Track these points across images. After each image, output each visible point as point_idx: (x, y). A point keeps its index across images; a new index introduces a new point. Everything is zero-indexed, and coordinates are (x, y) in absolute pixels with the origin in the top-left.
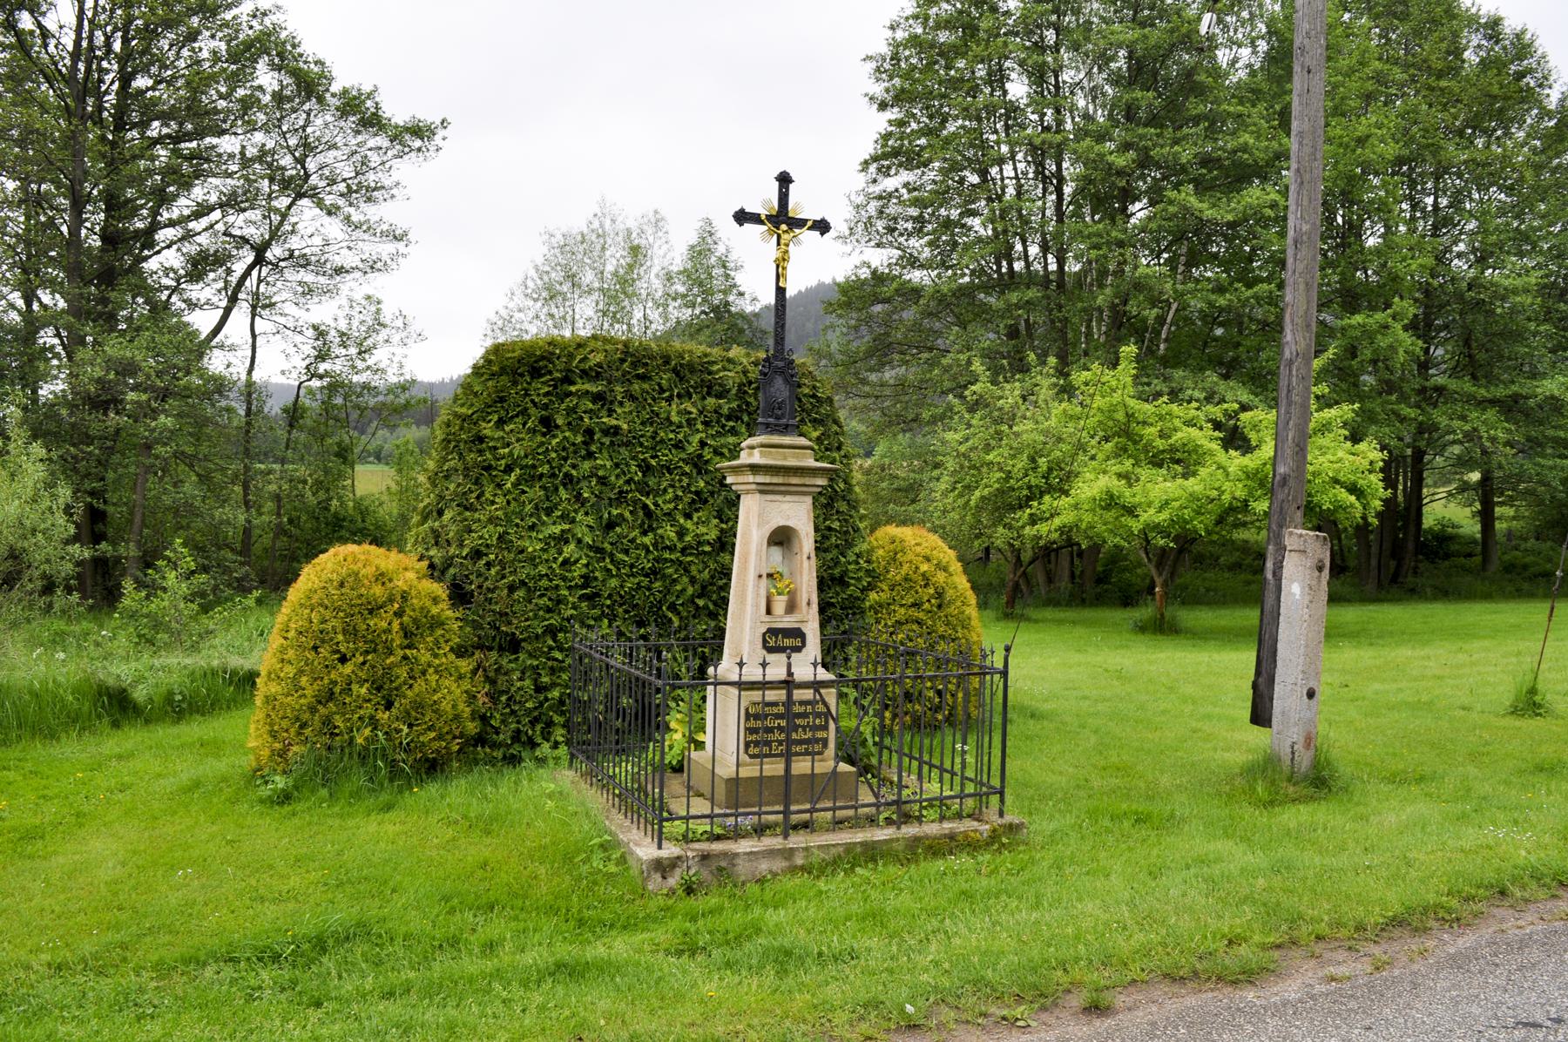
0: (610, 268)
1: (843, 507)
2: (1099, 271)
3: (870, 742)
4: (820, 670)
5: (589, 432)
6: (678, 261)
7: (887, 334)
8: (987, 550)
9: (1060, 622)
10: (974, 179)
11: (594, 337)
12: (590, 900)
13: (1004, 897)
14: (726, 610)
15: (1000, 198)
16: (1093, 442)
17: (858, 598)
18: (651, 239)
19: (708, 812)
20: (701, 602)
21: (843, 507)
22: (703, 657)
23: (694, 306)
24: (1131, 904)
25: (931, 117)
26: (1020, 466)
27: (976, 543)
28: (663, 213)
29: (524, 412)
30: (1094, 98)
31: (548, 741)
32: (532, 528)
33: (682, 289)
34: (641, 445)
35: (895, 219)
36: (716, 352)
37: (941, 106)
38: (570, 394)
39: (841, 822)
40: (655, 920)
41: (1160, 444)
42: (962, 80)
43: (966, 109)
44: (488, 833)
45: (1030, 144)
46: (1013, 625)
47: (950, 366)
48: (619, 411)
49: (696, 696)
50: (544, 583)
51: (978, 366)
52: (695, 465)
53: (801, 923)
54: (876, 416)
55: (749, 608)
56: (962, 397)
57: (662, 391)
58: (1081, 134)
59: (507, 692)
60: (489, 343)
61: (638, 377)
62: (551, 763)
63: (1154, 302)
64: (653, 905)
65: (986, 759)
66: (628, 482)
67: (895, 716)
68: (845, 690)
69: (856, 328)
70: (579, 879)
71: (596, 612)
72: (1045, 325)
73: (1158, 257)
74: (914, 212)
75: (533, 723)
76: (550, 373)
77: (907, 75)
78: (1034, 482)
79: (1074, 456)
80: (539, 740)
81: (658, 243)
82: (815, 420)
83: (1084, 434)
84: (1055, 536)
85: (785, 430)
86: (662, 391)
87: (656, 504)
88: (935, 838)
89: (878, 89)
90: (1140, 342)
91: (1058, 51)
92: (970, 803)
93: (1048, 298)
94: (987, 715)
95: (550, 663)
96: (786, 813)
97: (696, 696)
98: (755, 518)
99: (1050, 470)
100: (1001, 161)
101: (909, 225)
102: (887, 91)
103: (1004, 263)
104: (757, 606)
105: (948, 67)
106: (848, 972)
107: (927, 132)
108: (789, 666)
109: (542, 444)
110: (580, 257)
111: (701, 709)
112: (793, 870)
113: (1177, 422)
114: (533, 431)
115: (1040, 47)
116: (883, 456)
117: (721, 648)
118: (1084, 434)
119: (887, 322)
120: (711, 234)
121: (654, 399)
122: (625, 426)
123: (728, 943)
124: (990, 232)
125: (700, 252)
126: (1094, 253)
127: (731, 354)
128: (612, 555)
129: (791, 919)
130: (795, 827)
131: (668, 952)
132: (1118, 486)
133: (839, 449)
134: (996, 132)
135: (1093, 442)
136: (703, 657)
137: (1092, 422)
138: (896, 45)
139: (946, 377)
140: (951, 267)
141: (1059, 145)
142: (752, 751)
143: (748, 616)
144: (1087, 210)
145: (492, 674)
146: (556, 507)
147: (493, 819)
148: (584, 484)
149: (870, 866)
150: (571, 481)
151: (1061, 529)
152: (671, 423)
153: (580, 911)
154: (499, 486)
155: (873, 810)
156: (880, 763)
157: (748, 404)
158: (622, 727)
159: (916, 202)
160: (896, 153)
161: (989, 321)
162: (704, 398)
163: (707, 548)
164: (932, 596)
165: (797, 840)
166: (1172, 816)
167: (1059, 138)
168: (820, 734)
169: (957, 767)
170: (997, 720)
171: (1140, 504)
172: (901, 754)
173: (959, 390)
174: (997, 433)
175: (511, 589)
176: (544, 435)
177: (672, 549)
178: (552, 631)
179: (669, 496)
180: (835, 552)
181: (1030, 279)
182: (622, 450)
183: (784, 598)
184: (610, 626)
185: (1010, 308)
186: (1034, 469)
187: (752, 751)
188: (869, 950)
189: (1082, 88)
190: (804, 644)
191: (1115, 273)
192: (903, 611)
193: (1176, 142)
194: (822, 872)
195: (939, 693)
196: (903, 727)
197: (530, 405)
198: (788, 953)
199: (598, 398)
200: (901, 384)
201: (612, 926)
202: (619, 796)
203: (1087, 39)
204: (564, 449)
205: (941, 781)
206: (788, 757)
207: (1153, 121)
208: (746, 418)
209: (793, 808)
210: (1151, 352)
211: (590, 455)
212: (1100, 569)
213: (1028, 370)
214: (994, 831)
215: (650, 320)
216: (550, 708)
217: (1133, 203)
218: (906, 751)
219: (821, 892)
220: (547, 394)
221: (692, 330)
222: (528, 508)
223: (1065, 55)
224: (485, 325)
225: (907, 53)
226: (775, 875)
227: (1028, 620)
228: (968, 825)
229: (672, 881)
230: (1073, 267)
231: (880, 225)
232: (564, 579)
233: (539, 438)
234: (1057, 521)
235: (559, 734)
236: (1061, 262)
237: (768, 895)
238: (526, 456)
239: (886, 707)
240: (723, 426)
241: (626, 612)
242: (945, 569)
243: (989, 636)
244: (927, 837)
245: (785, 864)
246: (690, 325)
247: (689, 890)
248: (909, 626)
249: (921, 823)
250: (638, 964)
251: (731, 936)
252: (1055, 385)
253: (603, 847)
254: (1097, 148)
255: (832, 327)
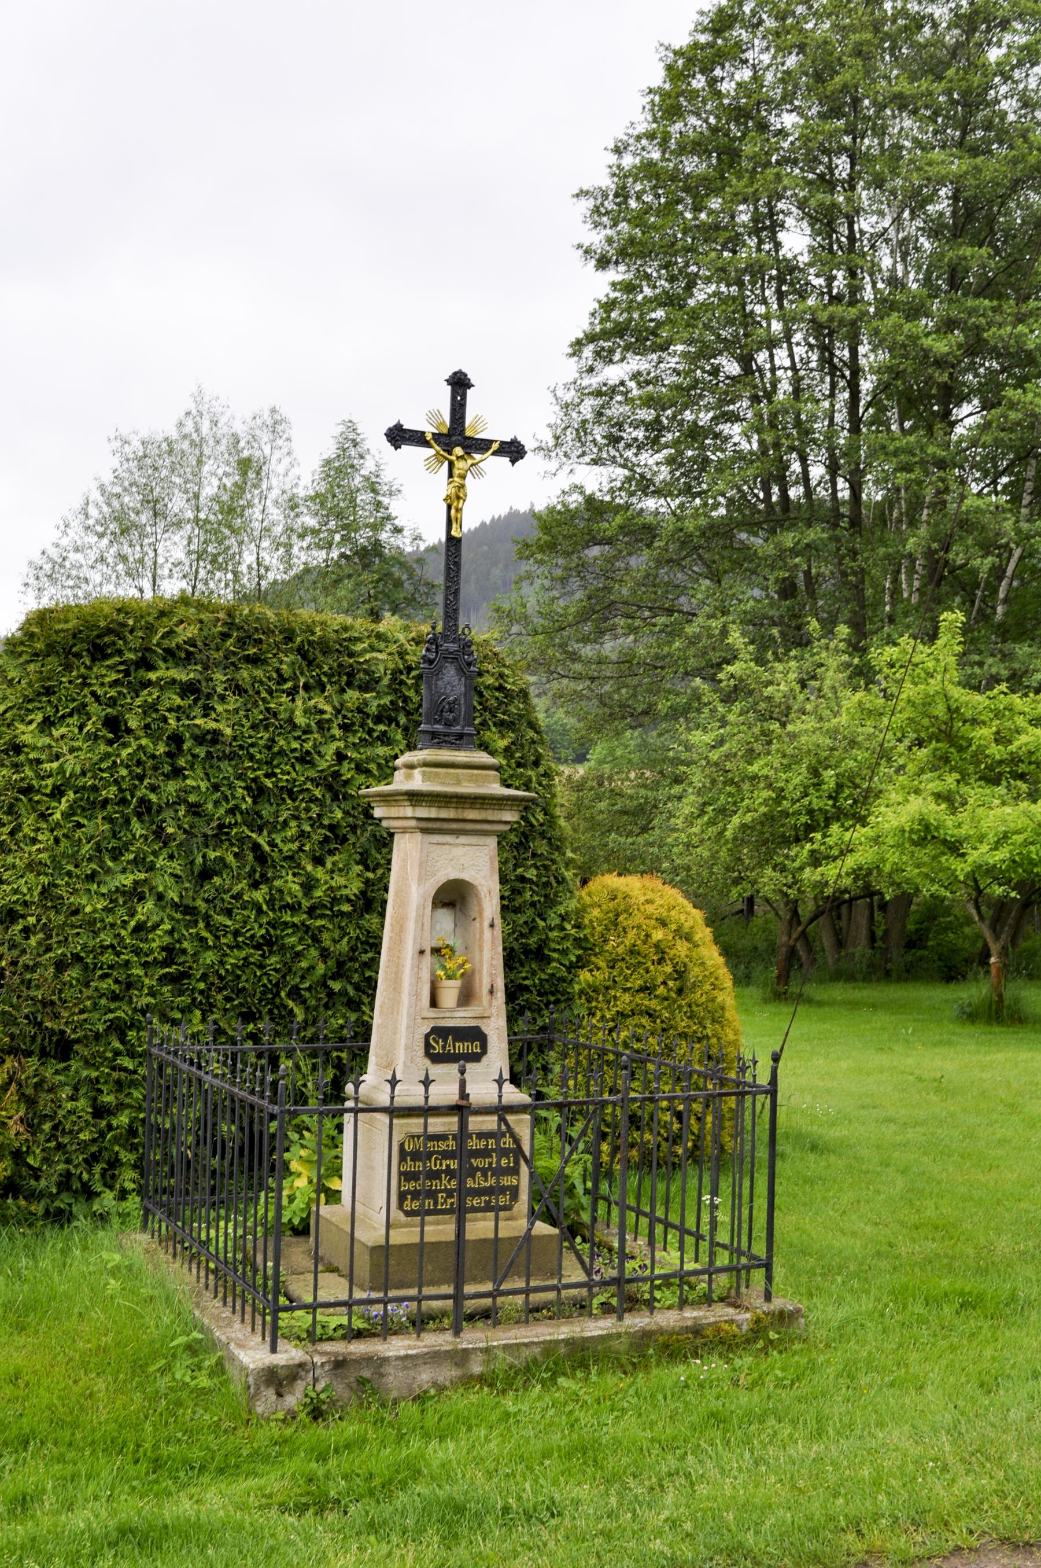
0: (209, 490)
1: (541, 847)
2: (909, 502)
3: (580, 1189)
4: (508, 1088)
5: (176, 739)
6: (306, 480)
7: (608, 589)
8: (751, 901)
9: (854, 1005)
10: (733, 368)
11: (184, 600)
12: (173, 1429)
13: (771, 1422)
14: (373, 997)
15: (769, 395)
16: (901, 748)
17: (563, 980)
18: (267, 450)
19: (344, 1296)
20: (336, 986)
21: (541, 847)
22: (339, 1065)
23: (329, 546)
24: (954, 1431)
25: (672, 279)
26: (796, 781)
27: (735, 892)
28: (284, 412)
29: (81, 709)
30: (905, 255)
31: (111, 1188)
32: (91, 877)
33: (311, 522)
34: (251, 758)
35: (620, 425)
36: (360, 624)
37: (687, 265)
38: (149, 683)
39: (537, 1310)
40: (266, 1459)
41: (996, 751)
42: (717, 227)
43: (723, 270)
44: (21, 1328)
45: (813, 321)
46: (787, 1009)
47: (698, 637)
48: (220, 708)
49: (329, 1124)
50: (108, 957)
51: (736, 638)
52: (330, 788)
53: (479, 1461)
54: (593, 707)
55: (405, 998)
56: (713, 679)
57: (282, 679)
58: (886, 306)
59: (52, 1118)
60: (32, 604)
61: (248, 659)
62: (115, 1221)
63: (987, 547)
64: (263, 1436)
65: (745, 1212)
66: (232, 811)
67: (615, 1150)
68: (543, 1113)
69: (564, 580)
70: (156, 1397)
71: (184, 1000)
72: (831, 573)
73: (994, 482)
74: (646, 414)
75: (90, 1162)
76: (120, 652)
77: (638, 220)
78: (817, 803)
79: (873, 769)
80: (98, 1187)
81: (277, 454)
82: (501, 724)
83: (890, 735)
84: (847, 882)
85: (459, 741)
86: (282, 679)
87: (272, 844)
88: (671, 1334)
89: (596, 239)
90: (969, 600)
91: (853, 188)
92: (723, 1280)
93: (838, 540)
94: (748, 1147)
95: (115, 1075)
96: (458, 1297)
97: (329, 1124)
98: (416, 868)
99: (840, 786)
100: (771, 344)
101: (640, 434)
102: (610, 241)
103: (775, 489)
104: (417, 995)
105: (697, 209)
106: (545, 1535)
107: (667, 300)
108: (463, 1084)
109: (107, 756)
110: (164, 473)
111: (335, 1143)
112: (468, 1381)
113: (1020, 721)
114: (95, 737)
115: (827, 182)
116: (601, 762)
117: (365, 1050)
118: (890, 735)
119: (608, 573)
120: (355, 444)
121: (270, 692)
122: (228, 731)
123: (371, 1493)
124: (755, 446)
125: (340, 468)
126: (902, 478)
127: (382, 627)
128: (207, 918)
129: (460, 1459)
130: (471, 1318)
131: (284, 1508)
132: (935, 811)
133: (536, 763)
134: (764, 302)
135: (901, 748)
136: (339, 1065)
137: (899, 719)
138: (620, 174)
139: (691, 651)
140: (699, 494)
141: (853, 323)
142: (408, 1205)
143: (404, 1010)
144: (893, 414)
145: (29, 1091)
146: (126, 847)
147: (29, 1307)
148: (167, 814)
149: (579, 1374)
150: (149, 810)
151: (856, 873)
152: (295, 727)
153: (155, 1447)
154: (43, 816)
155: (584, 1292)
156: (594, 1219)
157: (406, 699)
158: (219, 1168)
159: (649, 402)
160: (620, 330)
161: (754, 572)
162: (343, 691)
163: (346, 908)
164: (669, 977)
165: (474, 1337)
166: (1013, 1298)
167: (853, 312)
168: (507, 1181)
169: (705, 1229)
170: (762, 1153)
171: (967, 838)
172: (624, 1208)
173: (710, 671)
174: (764, 733)
175: (60, 966)
176: (110, 743)
177: (294, 908)
178: (118, 1028)
179: (292, 831)
180: (530, 912)
181: (811, 511)
182: (224, 764)
183: (456, 984)
184: (204, 1020)
185: (782, 554)
186: (817, 786)
187: (408, 1205)
188: (576, 1503)
189: (887, 241)
190: (484, 1050)
191: (932, 505)
192: (627, 997)
193: (1020, 319)
194: (509, 1384)
195: (679, 1116)
196: (627, 1163)
197: (89, 699)
198: (460, 1509)
199: (189, 689)
200: (627, 662)
201: (202, 1468)
202: (215, 1272)
203: (895, 172)
204: (139, 763)
205: (681, 1248)
206: (461, 1214)
207: (987, 288)
208: (403, 720)
209: (469, 1289)
210: (984, 617)
211: (177, 773)
212: (911, 927)
213: (809, 643)
214: (758, 1321)
215: (271, 558)
216: (116, 1140)
217: (958, 405)
218: (631, 1201)
219: (507, 1415)
220: (115, 683)
221: (326, 580)
222: (86, 849)
223: (864, 195)
224: (26, 569)
225: (638, 187)
226: (441, 1389)
227: (810, 1001)
228: (720, 1313)
229: (292, 1400)
230: (873, 494)
231: (598, 433)
232: (137, 952)
233: (103, 748)
234: (850, 862)
235: (128, 1178)
236: (856, 489)
237: (431, 1420)
238: (84, 773)
239: (604, 1136)
240: (370, 732)
241: (228, 999)
242: (688, 938)
243: (752, 1032)
244: (661, 1331)
245: (455, 1373)
246: (323, 573)
247: (317, 1414)
248: (635, 1020)
249: (652, 1310)
250: (240, 1528)
251: (376, 1482)
252: (848, 665)
253: (191, 1349)
254: (907, 327)
255: (529, 576)
